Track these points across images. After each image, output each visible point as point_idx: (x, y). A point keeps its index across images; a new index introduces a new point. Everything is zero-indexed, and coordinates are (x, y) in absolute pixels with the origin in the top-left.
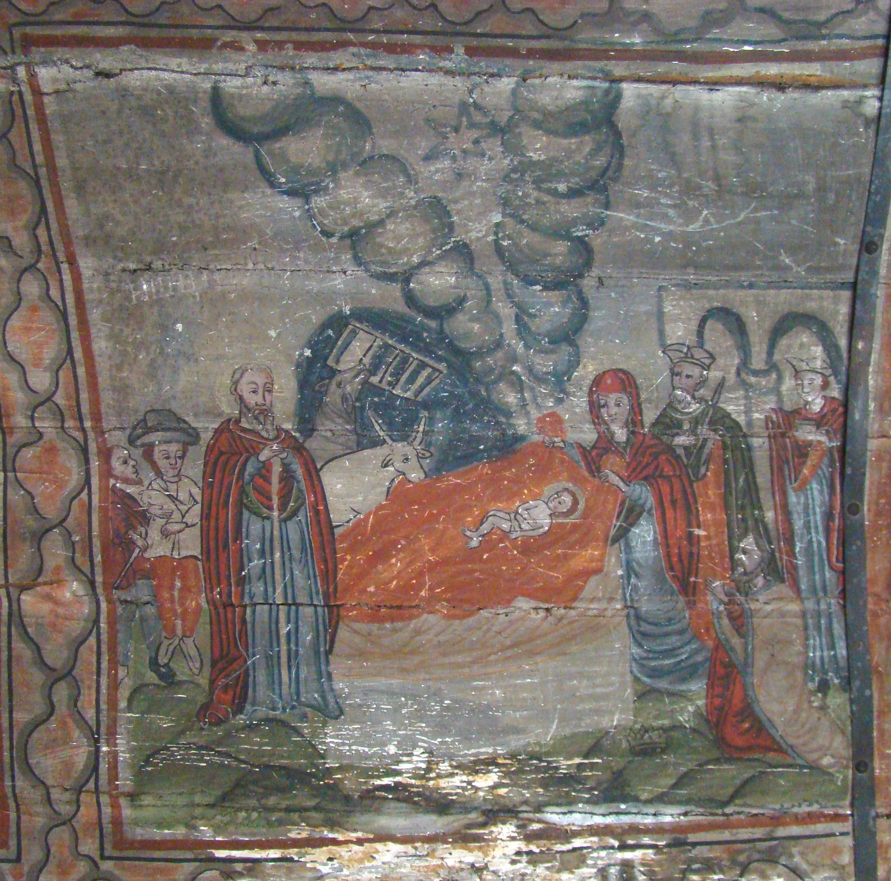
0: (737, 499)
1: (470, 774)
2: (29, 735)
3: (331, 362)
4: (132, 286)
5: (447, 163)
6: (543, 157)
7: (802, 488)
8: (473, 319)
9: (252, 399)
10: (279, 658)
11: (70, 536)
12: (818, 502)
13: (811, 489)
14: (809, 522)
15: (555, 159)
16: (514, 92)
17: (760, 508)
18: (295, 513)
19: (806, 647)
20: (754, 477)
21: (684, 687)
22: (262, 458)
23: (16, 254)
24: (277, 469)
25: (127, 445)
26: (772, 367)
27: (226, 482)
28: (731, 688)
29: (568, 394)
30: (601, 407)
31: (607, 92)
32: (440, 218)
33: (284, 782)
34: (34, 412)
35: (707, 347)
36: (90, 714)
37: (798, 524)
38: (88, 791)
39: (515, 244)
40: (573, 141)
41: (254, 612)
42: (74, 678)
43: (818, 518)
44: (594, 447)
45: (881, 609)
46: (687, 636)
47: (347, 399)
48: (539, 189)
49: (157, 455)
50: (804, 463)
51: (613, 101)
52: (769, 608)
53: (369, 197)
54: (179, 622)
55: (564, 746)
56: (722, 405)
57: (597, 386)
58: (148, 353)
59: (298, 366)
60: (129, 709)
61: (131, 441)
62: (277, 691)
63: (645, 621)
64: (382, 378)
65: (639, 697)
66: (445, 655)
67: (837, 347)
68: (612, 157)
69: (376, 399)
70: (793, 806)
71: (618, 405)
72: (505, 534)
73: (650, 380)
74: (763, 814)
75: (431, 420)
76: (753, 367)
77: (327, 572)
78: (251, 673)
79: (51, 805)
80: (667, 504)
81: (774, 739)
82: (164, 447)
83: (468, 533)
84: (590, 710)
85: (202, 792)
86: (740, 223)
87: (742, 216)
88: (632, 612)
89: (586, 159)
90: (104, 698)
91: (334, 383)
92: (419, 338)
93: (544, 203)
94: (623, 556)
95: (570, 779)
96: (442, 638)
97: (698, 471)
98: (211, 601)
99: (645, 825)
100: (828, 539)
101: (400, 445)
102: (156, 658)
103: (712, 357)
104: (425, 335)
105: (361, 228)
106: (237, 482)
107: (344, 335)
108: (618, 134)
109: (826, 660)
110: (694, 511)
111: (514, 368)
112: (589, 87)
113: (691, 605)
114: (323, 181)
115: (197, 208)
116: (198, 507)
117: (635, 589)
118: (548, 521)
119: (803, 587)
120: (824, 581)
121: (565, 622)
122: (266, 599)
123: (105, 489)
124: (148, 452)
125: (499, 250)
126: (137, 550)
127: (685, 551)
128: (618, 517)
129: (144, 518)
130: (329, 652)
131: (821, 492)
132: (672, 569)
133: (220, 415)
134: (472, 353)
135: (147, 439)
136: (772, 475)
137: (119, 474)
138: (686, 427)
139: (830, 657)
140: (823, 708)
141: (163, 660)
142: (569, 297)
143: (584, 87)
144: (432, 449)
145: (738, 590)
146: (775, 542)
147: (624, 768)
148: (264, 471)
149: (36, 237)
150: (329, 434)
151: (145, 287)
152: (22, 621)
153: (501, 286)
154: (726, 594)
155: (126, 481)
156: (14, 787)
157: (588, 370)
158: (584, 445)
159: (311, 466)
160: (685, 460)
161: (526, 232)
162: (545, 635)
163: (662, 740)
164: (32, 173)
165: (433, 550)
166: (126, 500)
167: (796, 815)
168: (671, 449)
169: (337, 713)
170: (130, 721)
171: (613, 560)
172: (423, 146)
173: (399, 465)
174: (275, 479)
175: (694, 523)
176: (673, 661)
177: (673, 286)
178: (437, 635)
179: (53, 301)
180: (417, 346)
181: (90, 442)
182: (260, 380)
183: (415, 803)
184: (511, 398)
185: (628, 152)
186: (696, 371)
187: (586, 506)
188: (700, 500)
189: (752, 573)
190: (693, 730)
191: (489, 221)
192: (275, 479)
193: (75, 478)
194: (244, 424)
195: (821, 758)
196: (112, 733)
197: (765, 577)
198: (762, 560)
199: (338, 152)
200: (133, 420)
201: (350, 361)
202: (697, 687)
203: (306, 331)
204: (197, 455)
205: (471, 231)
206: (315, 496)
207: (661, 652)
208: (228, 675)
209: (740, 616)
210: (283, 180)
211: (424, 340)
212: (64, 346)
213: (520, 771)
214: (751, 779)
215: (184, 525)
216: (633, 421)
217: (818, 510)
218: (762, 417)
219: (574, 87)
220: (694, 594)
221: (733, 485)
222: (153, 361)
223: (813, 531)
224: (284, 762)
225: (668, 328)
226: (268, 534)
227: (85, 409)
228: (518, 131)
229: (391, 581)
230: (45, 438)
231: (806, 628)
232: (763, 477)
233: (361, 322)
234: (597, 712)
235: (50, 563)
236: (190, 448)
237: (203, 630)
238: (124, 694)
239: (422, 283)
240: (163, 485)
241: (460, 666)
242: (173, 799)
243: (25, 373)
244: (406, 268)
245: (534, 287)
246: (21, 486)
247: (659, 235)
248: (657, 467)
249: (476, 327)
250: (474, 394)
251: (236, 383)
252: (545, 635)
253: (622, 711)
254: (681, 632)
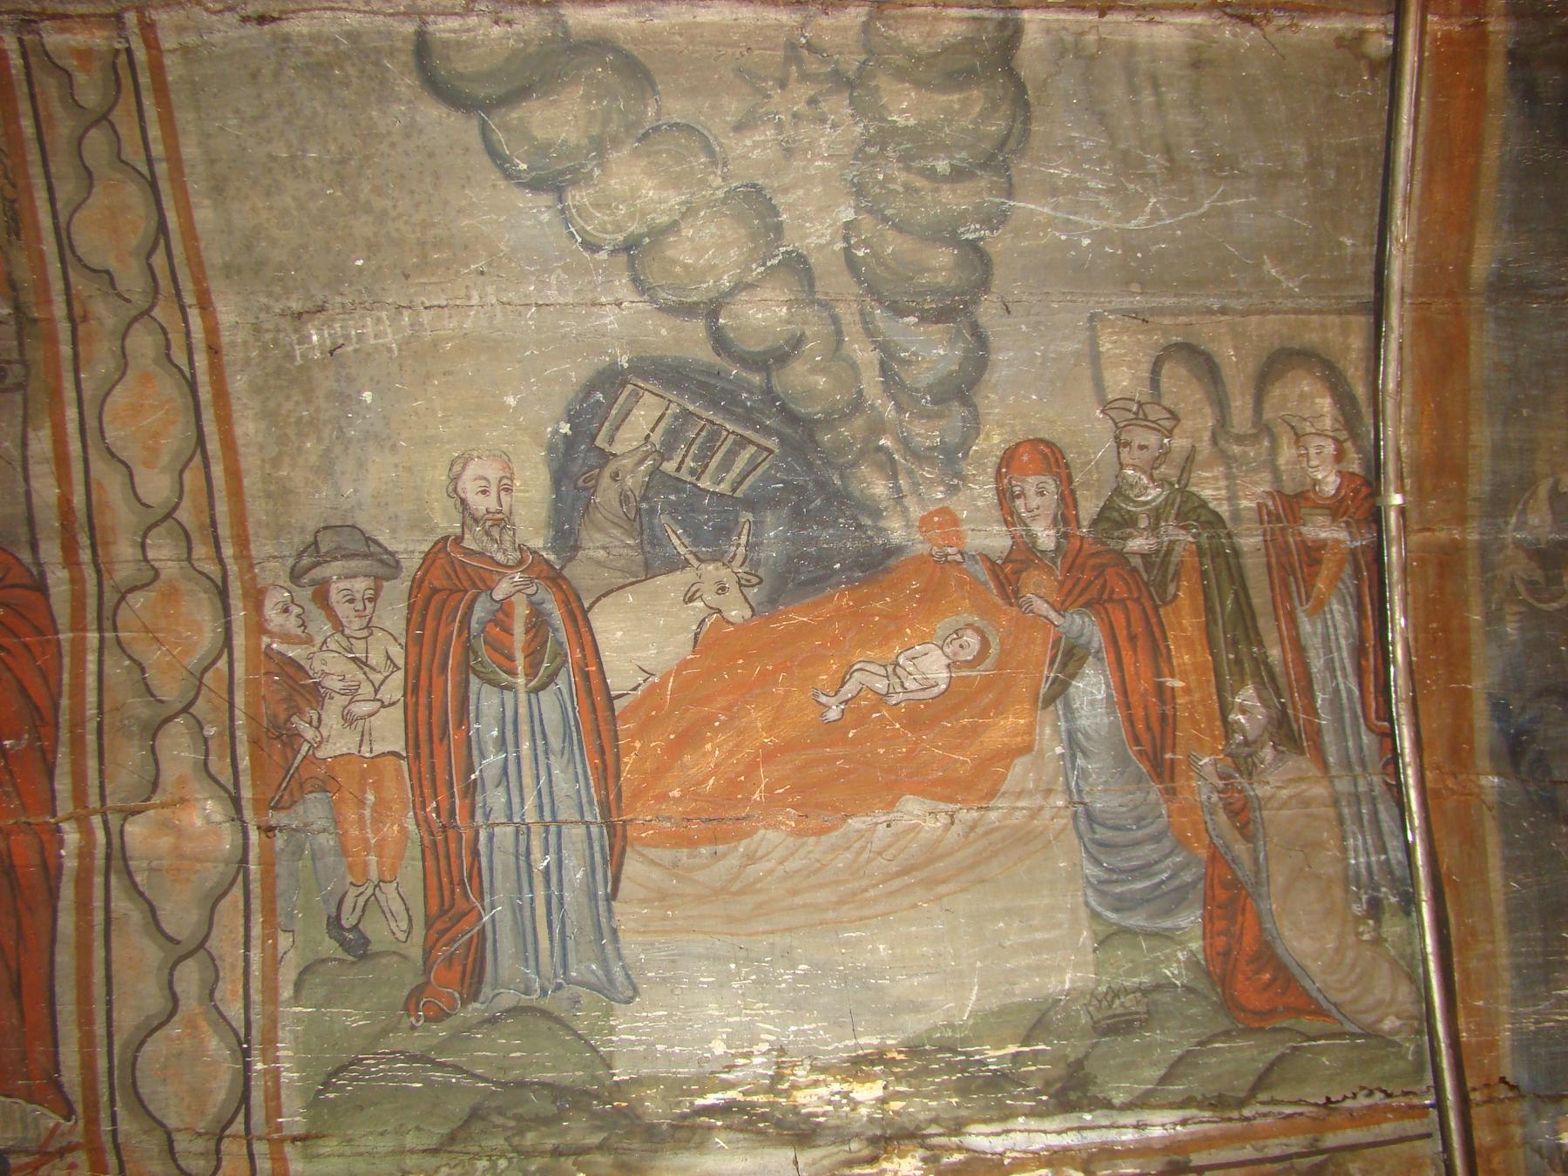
0: (1225, 633)
1: (844, 1080)
2: (138, 1049)
3: (600, 441)
4: (294, 337)
5: (770, 133)
6: (912, 122)
7: (1319, 608)
8: (815, 370)
9: (480, 504)
10: (533, 909)
11: (202, 728)
12: (1342, 631)
13: (1331, 612)
14: (1332, 660)
15: (931, 125)
16: (866, 27)
17: (1261, 644)
18: (552, 677)
19: (1344, 850)
20: (1248, 597)
21: (1168, 923)
22: (499, 594)
23: (119, 295)
24: (521, 611)
25: (288, 584)
26: (1263, 429)
27: (442, 632)
28: (1240, 919)
29: (964, 478)
30: (1014, 497)
31: (1002, 24)
32: (761, 217)
33: (550, 1109)
34: (145, 536)
35: (1166, 402)
36: (235, 1011)
37: (1317, 664)
38: (235, 1137)
39: (875, 254)
40: (956, 97)
41: (491, 837)
42: (210, 954)
43: (1345, 654)
44: (1007, 560)
45: (1447, 788)
46: (1167, 844)
47: (627, 497)
48: (908, 169)
49: (335, 597)
50: (1317, 574)
51: (1011, 35)
52: (1285, 793)
53: (653, 188)
54: (373, 859)
55: (992, 1023)
56: (1194, 489)
57: (1007, 467)
58: (319, 440)
59: (551, 448)
60: (296, 999)
61: (295, 576)
62: (532, 962)
63: (1103, 825)
64: (682, 462)
65: (1101, 943)
66: (794, 892)
67: (1352, 399)
68: (1014, 121)
69: (673, 497)
70: (1345, 1098)
71: (1042, 494)
72: (882, 698)
73: (1087, 454)
74: (1301, 1114)
75: (758, 525)
76: (1234, 431)
77: (605, 769)
78: (489, 935)
79: (175, 1160)
80: (1123, 642)
81: (1309, 996)
82: (342, 585)
83: (823, 699)
84: (1029, 967)
85: (418, 1128)
86: (1204, 215)
87: (1206, 206)
88: (1080, 808)
89: (975, 122)
90: (256, 984)
91: (607, 473)
92: (735, 400)
93: (917, 191)
94: (1062, 724)
95: (999, 1081)
96: (792, 865)
97: (1165, 591)
98: (422, 822)
99: (1122, 1143)
100: (1361, 685)
101: (711, 567)
102: (338, 917)
103: (1174, 416)
104: (744, 395)
105: (642, 236)
106: (459, 635)
107: (621, 400)
108: (1021, 87)
109: (1375, 868)
110: (1164, 651)
111: (882, 442)
112: (975, 19)
113: (1171, 793)
114: (583, 166)
115: (393, 213)
116: (400, 675)
117: (1084, 774)
118: (945, 675)
119: (1331, 760)
120: (1361, 749)
121: (980, 830)
122: (510, 817)
123: (253, 652)
124: (321, 595)
125: (851, 263)
126: (305, 747)
127: (1155, 712)
128: (1052, 663)
129: (316, 694)
130: (613, 896)
131: (1346, 615)
132: (1136, 740)
133: (432, 530)
134: (818, 421)
135: (317, 573)
136: (1272, 589)
137: (275, 629)
138: (1143, 524)
139: (1378, 862)
140: (1378, 941)
141: (348, 921)
142: (959, 331)
143: (968, 19)
144: (761, 572)
145: (1238, 770)
146: (1286, 694)
147: (1087, 1056)
148: (500, 616)
149: (150, 267)
150: (601, 554)
151: (315, 338)
152: (127, 866)
153: (857, 318)
154: (1221, 778)
155: (287, 638)
156: (114, 1133)
157: (993, 441)
158: (992, 556)
159: (574, 605)
160: (1145, 576)
161: (891, 234)
162: (951, 853)
163: (1142, 1009)
164: (145, 170)
165: (769, 728)
166: (287, 669)
167: (1350, 1111)
168: (1122, 557)
169: (630, 993)
170: (298, 1019)
171: (1048, 731)
172: (733, 107)
173: (710, 598)
174: (519, 628)
175: (1166, 670)
176: (1147, 883)
177: (1111, 312)
178: (781, 863)
179: (177, 367)
180: (733, 413)
181: (231, 578)
182: (493, 472)
183: (760, 1132)
184: (880, 488)
185: (1036, 111)
186: (1152, 439)
187: (1002, 651)
188: (1170, 634)
189: (1255, 742)
190: (1189, 989)
191: (835, 220)
192: (519, 628)
193: (207, 637)
194: (469, 543)
195: (1380, 1020)
196: (270, 1041)
197: (1274, 747)
198: (1270, 719)
199: (606, 122)
200: (298, 541)
201: (629, 440)
202: (1189, 920)
203: (561, 398)
204: (396, 591)
205: (808, 236)
206: (583, 650)
207: (1131, 870)
208: (454, 940)
209: (1243, 808)
210: (525, 166)
211: (742, 404)
212: (192, 432)
213: (926, 1071)
214: (1281, 1058)
215: (378, 704)
216: (1065, 516)
217: (1343, 642)
218: (1253, 505)
219: (954, 19)
220: (1172, 779)
221: (1218, 608)
222: (328, 450)
223: (1339, 673)
224: (548, 1076)
225: (1108, 375)
226: (509, 713)
227: (224, 531)
228: (873, 83)
229: (706, 780)
230: (162, 577)
231: (1341, 821)
232: (1260, 598)
233: (646, 380)
234: (1039, 969)
235: (170, 773)
236: (385, 584)
237: (412, 871)
238: (287, 976)
239: (737, 316)
240: (345, 643)
241: (818, 908)
242: (370, 1142)
243: (131, 475)
244: (712, 295)
245: (906, 320)
246: (124, 651)
247: (1088, 236)
248: (1104, 586)
249: (821, 381)
250: (822, 485)
251: (455, 479)
252: (951, 853)
253: (1077, 966)
254: (1157, 838)
